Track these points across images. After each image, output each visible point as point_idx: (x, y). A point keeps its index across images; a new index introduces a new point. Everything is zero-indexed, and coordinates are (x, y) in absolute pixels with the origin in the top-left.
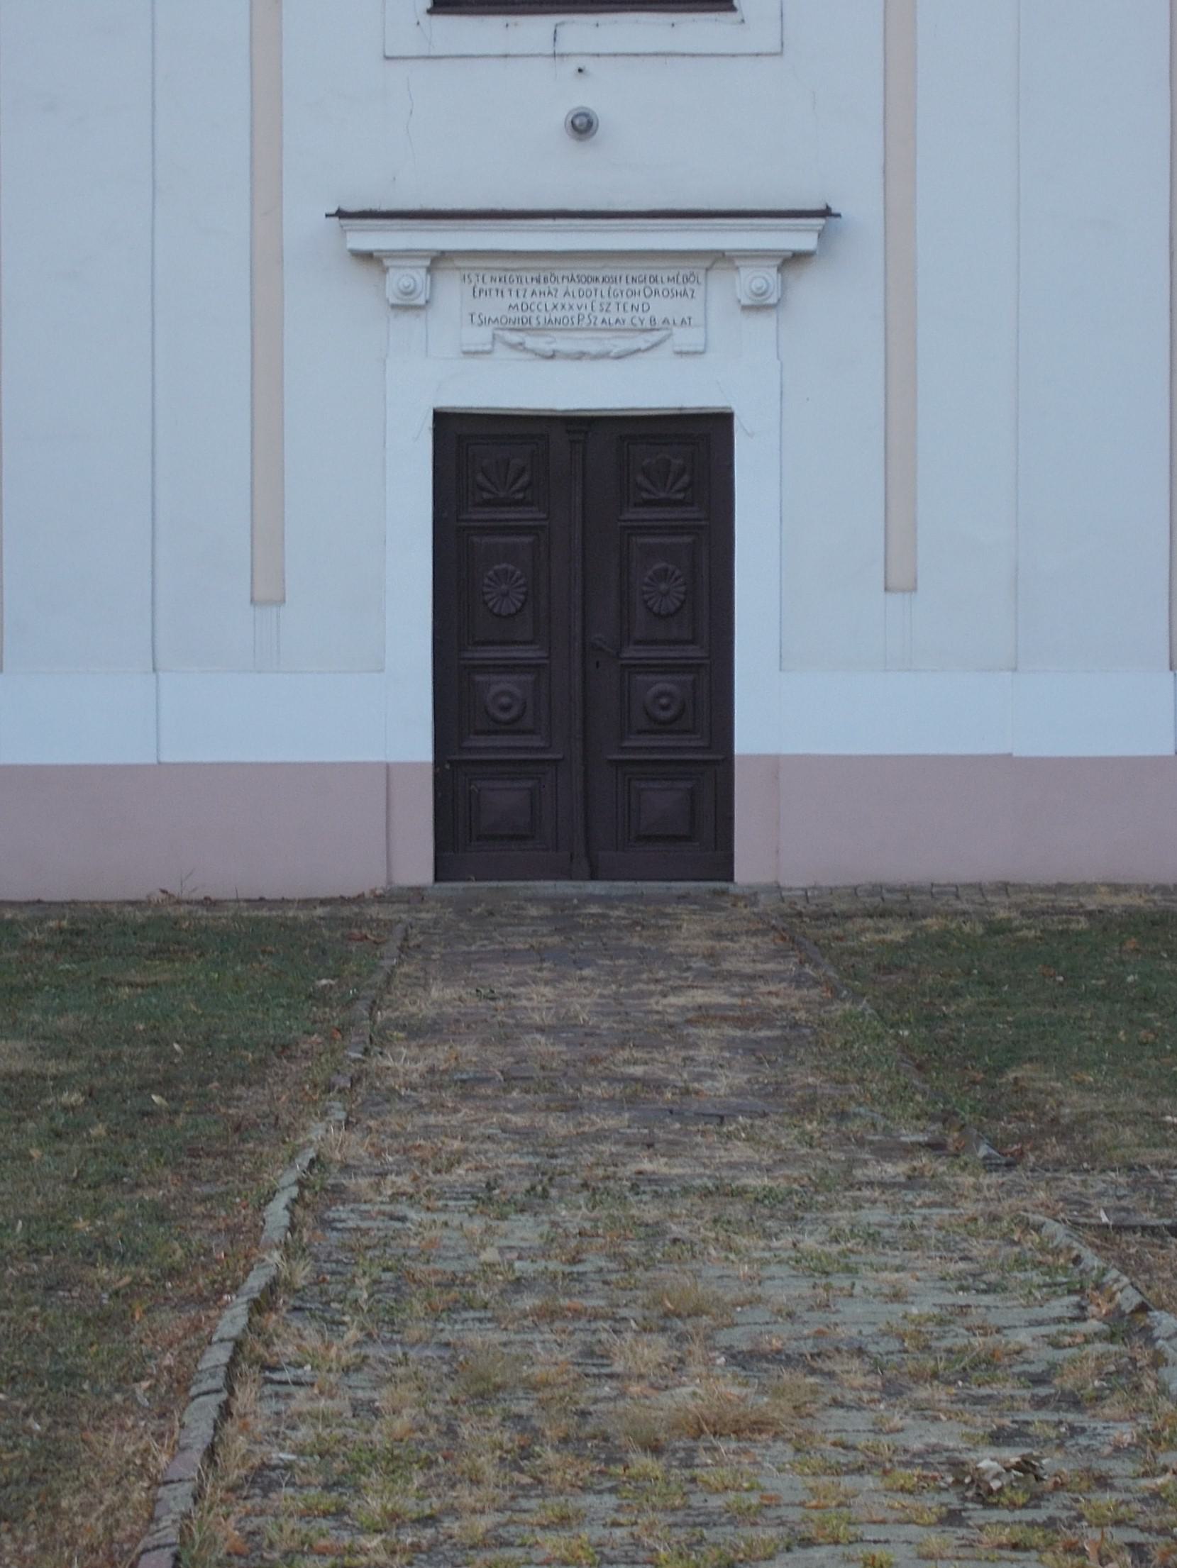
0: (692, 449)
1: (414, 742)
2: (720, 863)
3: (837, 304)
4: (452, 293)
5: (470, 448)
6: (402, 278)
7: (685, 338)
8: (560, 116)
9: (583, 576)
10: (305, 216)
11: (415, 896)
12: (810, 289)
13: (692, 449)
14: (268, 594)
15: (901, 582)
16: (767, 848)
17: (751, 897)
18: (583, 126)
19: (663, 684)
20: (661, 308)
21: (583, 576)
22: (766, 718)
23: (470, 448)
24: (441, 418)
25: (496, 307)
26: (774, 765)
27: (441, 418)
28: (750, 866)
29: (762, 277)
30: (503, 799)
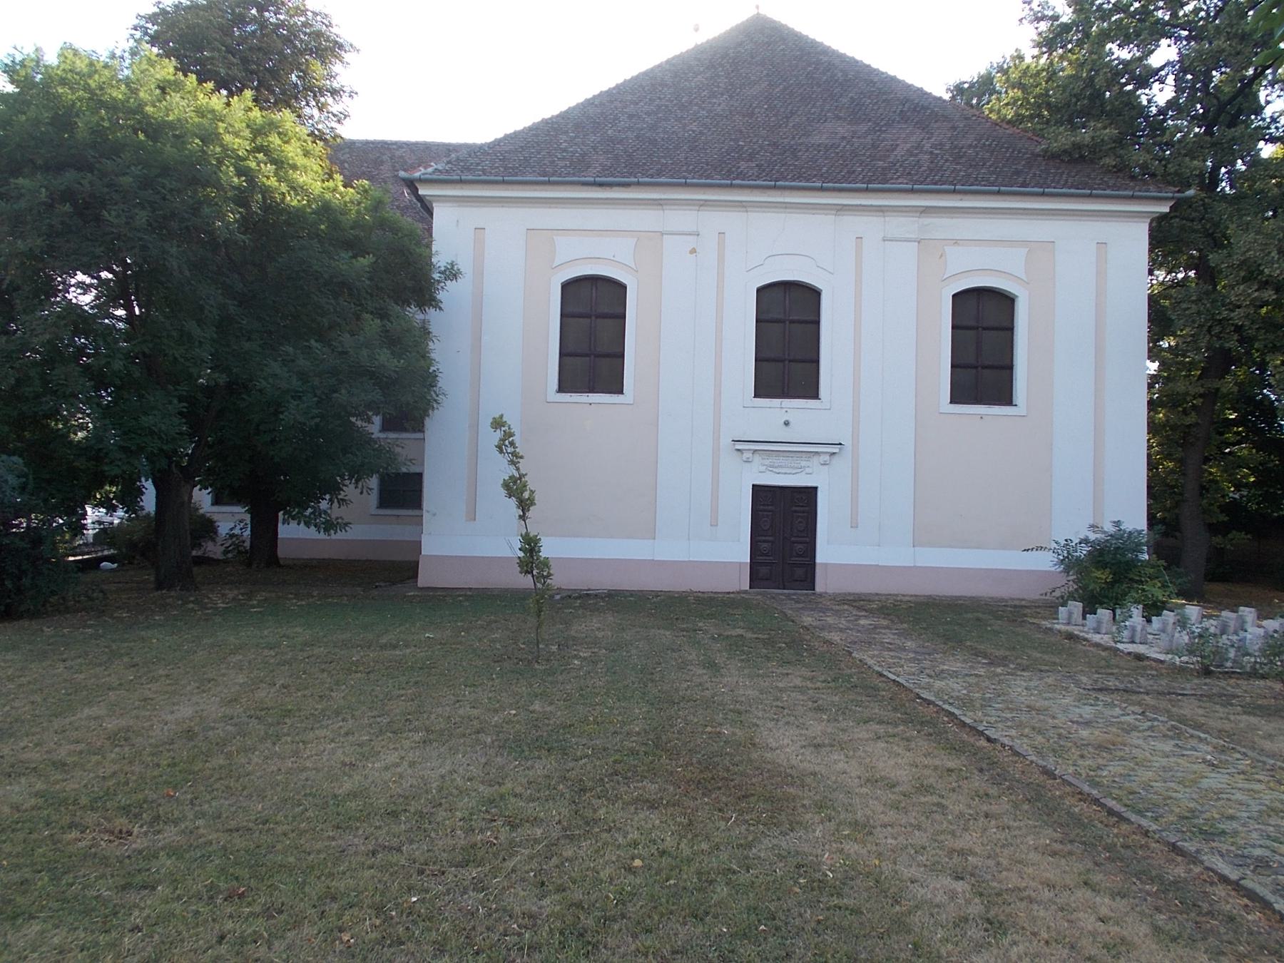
0: (809, 494)
1: (747, 559)
2: (812, 586)
3: (842, 465)
4: (757, 458)
5: (760, 492)
6: (746, 455)
7: (808, 470)
8: (791, 420)
9: (784, 520)
10: (726, 441)
11: (745, 592)
12: (835, 459)
13: (809, 494)
14: (714, 524)
15: (854, 526)
16: (823, 584)
17: (821, 595)
18: (787, 424)
19: (800, 546)
20: (803, 464)
21: (784, 520)
22: (826, 553)
23: (760, 492)
24: (816, 488)
25: (767, 462)
26: (826, 565)
27: (816, 488)
28: (819, 587)
29: (827, 457)
30: (764, 571)
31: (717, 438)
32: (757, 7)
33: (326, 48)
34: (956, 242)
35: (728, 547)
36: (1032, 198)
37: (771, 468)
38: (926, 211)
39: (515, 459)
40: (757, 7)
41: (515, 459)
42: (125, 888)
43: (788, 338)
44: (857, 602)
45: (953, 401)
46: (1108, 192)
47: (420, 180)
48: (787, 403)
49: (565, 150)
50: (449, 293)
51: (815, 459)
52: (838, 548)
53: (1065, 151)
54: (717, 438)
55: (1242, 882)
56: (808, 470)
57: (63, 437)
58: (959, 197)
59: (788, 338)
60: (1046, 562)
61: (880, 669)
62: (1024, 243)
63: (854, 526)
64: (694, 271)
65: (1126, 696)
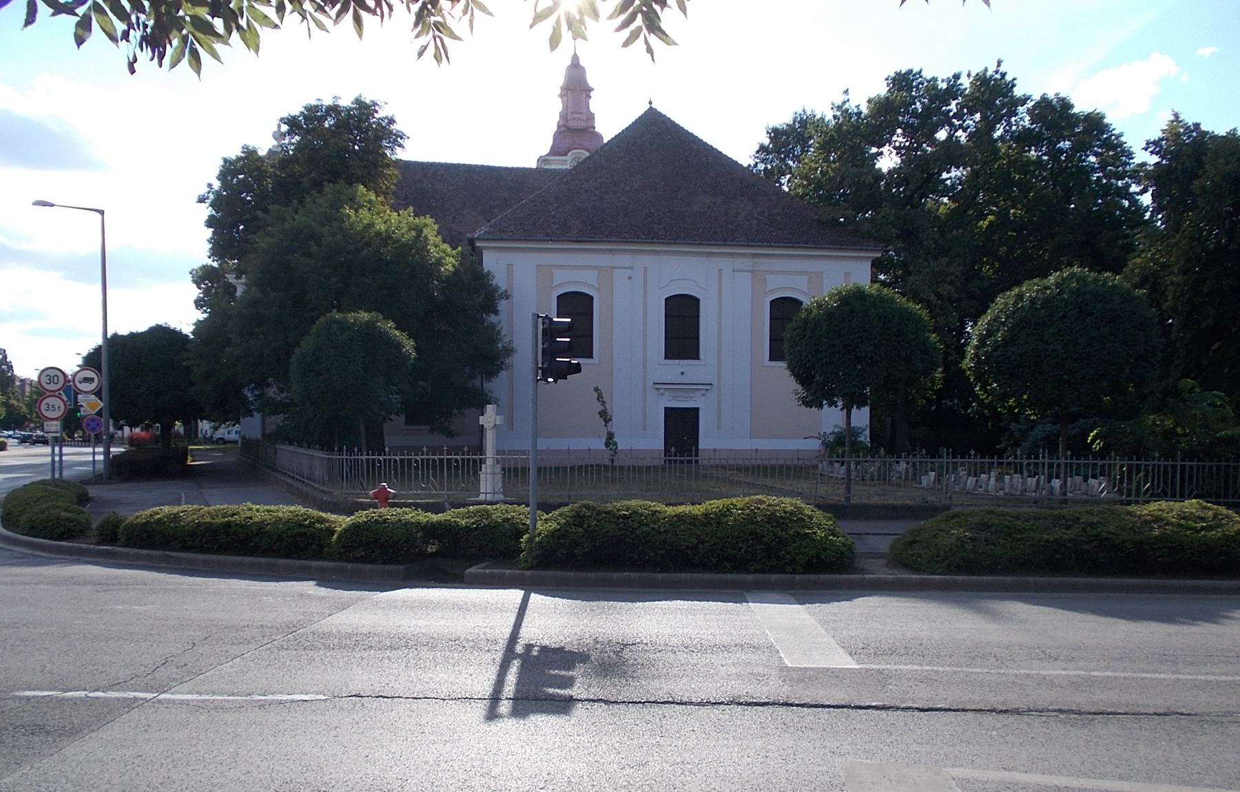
0: (696, 411)
9: (682, 426)
10: (650, 384)
13: (696, 411)
21: (682, 426)
22: (704, 443)
31: (644, 383)
32: (650, 103)
33: (364, 109)
34: (772, 273)
35: (653, 440)
37: (674, 398)
38: (755, 255)
40: (650, 103)
43: (682, 326)
47: (478, 239)
48: (682, 362)
49: (554, 217)
50: (502, 305)
51: (698, 393)
52: (707, 441)
54: (644, 383)
55: (538, 10)
59: (682, 326)
60: (815, 445)
61: (1129, 508)
63: (719, 428)
64: (630, 287)
65: (1137, 710)
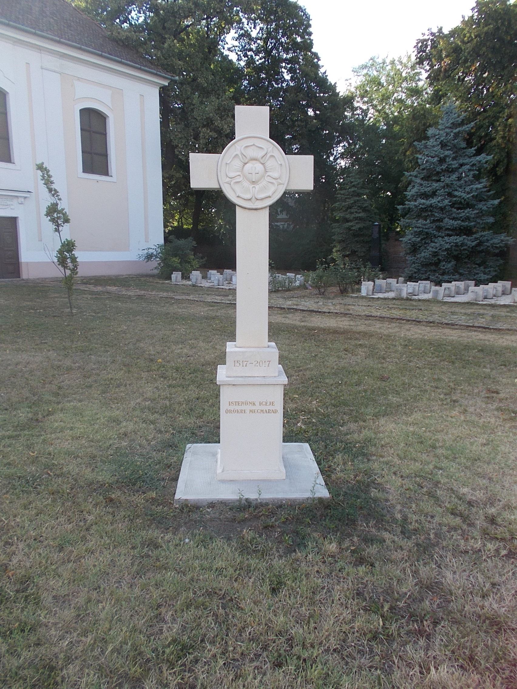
2: (19, 277)
7: (12, 207)
13: (13, 221)
20: (9, 203)
26: (27, 263)
29: (23, 200)
34: (79, 79)
36: (115, 63)
39: (50, 190)
41: (53, 192)
42: (420, 666)
44: (98, 281)
45: (85, 171)
46: (146, 68)
51: (15, 201)
53: (120, 40)
56: (12, 207)
57: (345, 110)
58: (81, 52)
62: (110, 87)
